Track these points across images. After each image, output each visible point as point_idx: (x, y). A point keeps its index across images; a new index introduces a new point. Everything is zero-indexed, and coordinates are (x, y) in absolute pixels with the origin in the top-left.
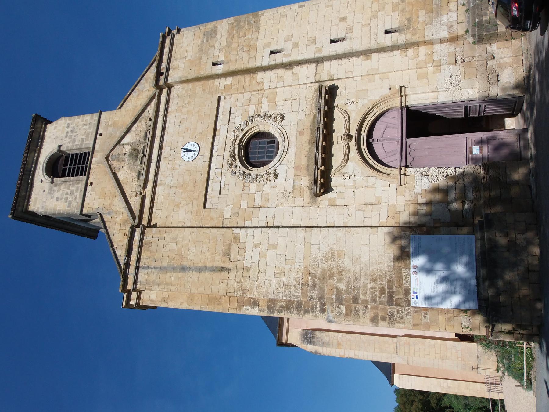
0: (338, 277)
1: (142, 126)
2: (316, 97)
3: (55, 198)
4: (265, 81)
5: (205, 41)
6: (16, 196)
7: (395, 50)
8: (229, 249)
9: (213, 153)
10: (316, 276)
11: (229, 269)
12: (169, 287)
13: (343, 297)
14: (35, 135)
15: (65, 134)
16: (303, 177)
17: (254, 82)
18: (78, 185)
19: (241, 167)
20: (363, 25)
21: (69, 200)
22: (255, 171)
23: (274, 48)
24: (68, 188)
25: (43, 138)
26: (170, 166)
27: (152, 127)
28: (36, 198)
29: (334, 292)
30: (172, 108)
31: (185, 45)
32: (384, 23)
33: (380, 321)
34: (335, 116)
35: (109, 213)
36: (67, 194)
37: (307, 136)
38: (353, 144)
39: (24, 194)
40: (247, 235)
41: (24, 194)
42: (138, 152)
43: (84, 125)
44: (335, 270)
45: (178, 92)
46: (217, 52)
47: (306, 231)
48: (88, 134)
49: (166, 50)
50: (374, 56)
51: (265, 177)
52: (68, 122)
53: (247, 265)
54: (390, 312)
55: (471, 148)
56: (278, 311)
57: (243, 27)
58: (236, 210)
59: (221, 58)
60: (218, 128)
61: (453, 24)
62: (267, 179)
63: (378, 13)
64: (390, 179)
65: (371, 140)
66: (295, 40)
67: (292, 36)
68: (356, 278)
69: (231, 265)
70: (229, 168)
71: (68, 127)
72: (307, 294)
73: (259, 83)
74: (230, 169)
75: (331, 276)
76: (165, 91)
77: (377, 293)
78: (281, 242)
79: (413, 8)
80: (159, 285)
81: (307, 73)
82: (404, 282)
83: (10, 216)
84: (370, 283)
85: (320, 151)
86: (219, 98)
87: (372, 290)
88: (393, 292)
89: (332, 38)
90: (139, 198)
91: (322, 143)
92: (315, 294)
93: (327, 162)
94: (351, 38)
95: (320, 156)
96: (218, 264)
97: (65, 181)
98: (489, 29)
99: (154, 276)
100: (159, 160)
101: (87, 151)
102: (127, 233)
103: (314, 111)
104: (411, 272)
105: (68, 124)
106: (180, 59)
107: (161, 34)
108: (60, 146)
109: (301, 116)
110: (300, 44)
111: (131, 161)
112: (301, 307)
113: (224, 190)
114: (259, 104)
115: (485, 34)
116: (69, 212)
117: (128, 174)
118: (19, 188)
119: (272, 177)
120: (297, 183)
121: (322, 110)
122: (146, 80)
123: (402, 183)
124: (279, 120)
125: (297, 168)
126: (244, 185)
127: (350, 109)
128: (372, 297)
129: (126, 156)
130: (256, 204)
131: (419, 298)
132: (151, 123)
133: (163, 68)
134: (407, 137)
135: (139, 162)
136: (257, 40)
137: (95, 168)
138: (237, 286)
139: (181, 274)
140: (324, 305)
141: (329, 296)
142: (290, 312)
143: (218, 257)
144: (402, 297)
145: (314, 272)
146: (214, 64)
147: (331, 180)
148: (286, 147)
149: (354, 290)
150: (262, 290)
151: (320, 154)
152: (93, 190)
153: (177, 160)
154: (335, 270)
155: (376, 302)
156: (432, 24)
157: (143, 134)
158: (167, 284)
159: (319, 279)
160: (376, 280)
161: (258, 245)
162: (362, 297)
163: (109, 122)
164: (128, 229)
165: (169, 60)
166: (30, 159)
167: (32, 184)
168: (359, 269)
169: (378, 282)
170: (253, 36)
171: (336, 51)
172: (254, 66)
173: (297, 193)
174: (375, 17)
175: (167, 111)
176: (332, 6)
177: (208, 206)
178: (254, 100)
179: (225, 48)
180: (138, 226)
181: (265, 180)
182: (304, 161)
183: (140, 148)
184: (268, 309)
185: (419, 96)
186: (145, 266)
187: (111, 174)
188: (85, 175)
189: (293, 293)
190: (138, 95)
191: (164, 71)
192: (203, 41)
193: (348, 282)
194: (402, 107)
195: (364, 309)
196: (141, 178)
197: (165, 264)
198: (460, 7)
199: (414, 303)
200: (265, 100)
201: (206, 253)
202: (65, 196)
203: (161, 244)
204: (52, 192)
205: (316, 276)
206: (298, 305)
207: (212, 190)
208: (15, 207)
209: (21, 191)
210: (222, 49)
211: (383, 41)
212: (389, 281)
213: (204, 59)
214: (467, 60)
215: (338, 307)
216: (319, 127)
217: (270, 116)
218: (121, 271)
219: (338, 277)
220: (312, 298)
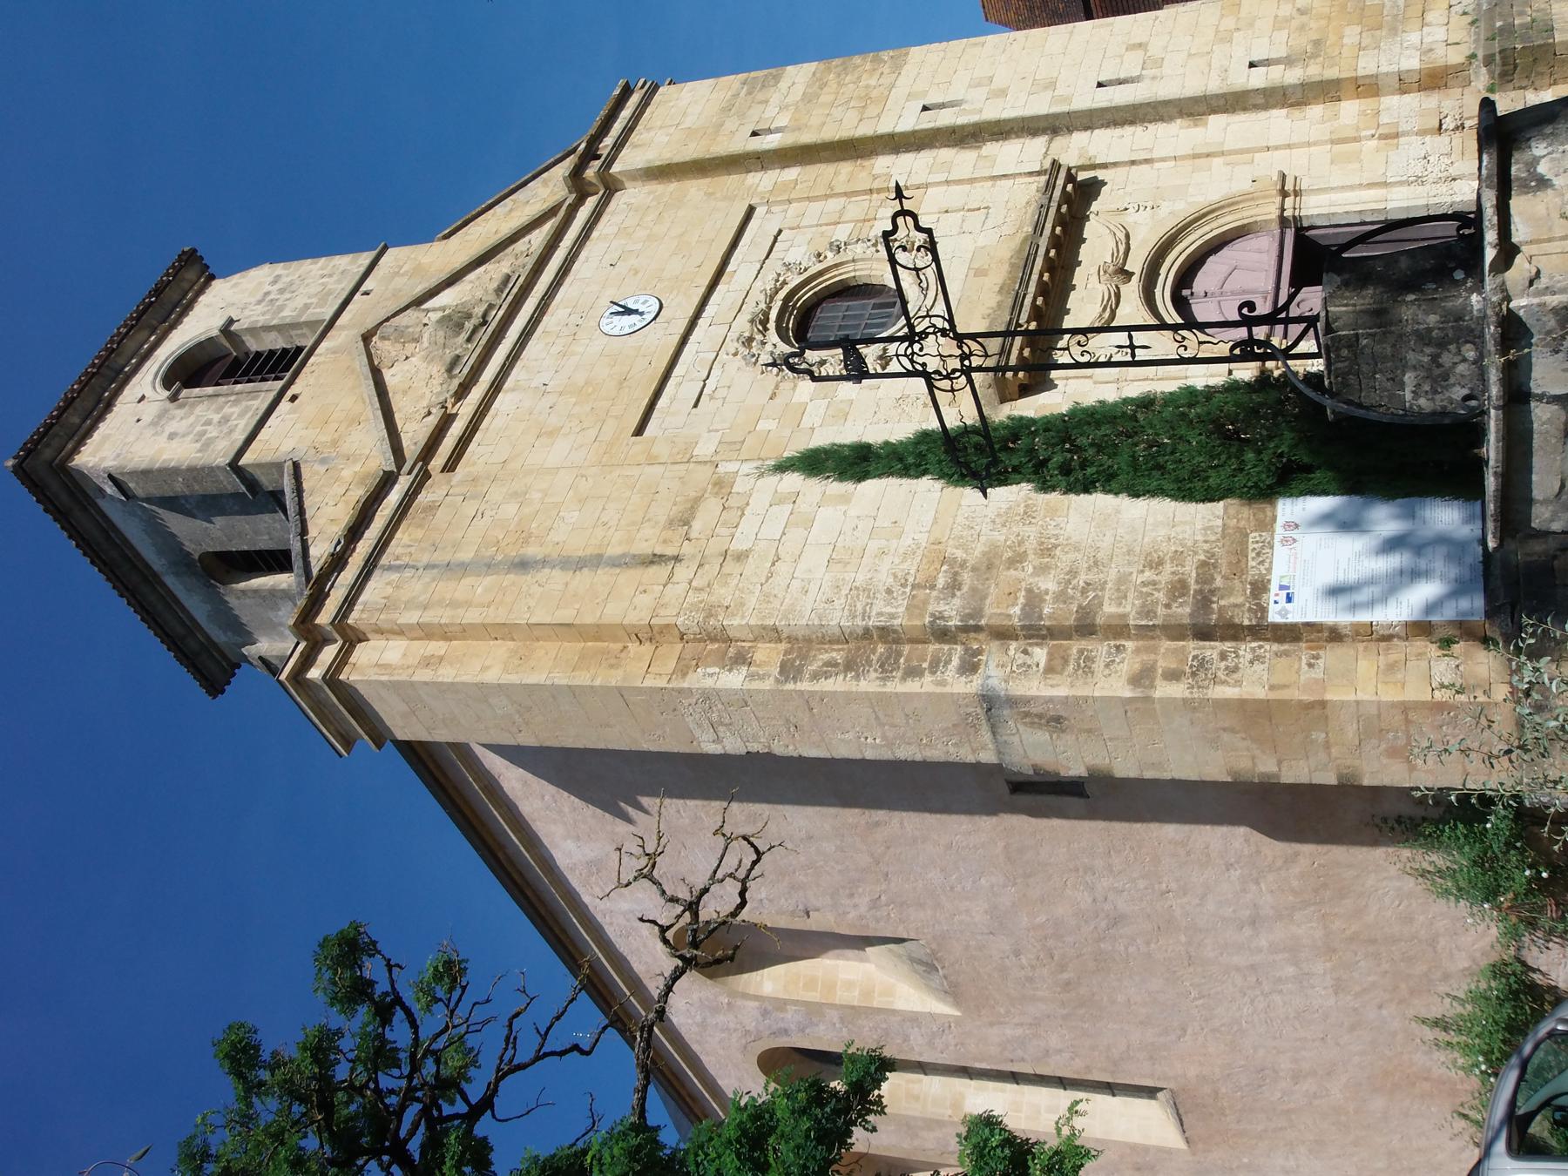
3: (166, 434)
6: (52, 417)
7: (1274, 107)
14: (171, 294)
15: (259, 296)
17: (864, 174)
20: (1190, 55)
39: (76, 420)
41: (76, 420)
44: (1031, 545)
49: (626, 113)
53: (738, 545)
56: (815, 676)
68: (1096, 563)
69: (687, 549)
75: (1017, 560)
76: (591, 202)
82: (1252, 563)
83: (10, 463)
85: (1032, 289)
86: (751, 210)
88: (1212, 592)
94: (1154, 78)
104: (1277, 538)
107: (622, 82)
108: (231, 321)
111: (441, 333)
112: (897, 661)
115: (1519, 46)
118: (70, 402)
127: (1127, 221)
128: (1144, 605)
131: (1295, 599)
138: (692, 598)
142: (857, 677)
144: (1240, 600)
145: (960, 554)
146: (754, 134)
149: (1084, 592)
150: (776, 603)
154: (1031, 545)
156: (1378, 47)
159: (974, 569)
160: (1160, 563)
166: (130, 345)
167: (109, 406)
168: (1108, 540)
169: (1168, 568)
177: (648, 432)
184: (781, 673)
185: (1334, 196)
187: (367, 370)
194: (1283, 222)
195: (1109, 653)
198: (1455, 19)
199: (1279, 613)
202: (199, 428)
203: (470, 509)
206: (888, 658)
209: (70, 410)
210: (787, 107)
215: (1025, 652)
218: (308, 581)
219: (1037, 562)
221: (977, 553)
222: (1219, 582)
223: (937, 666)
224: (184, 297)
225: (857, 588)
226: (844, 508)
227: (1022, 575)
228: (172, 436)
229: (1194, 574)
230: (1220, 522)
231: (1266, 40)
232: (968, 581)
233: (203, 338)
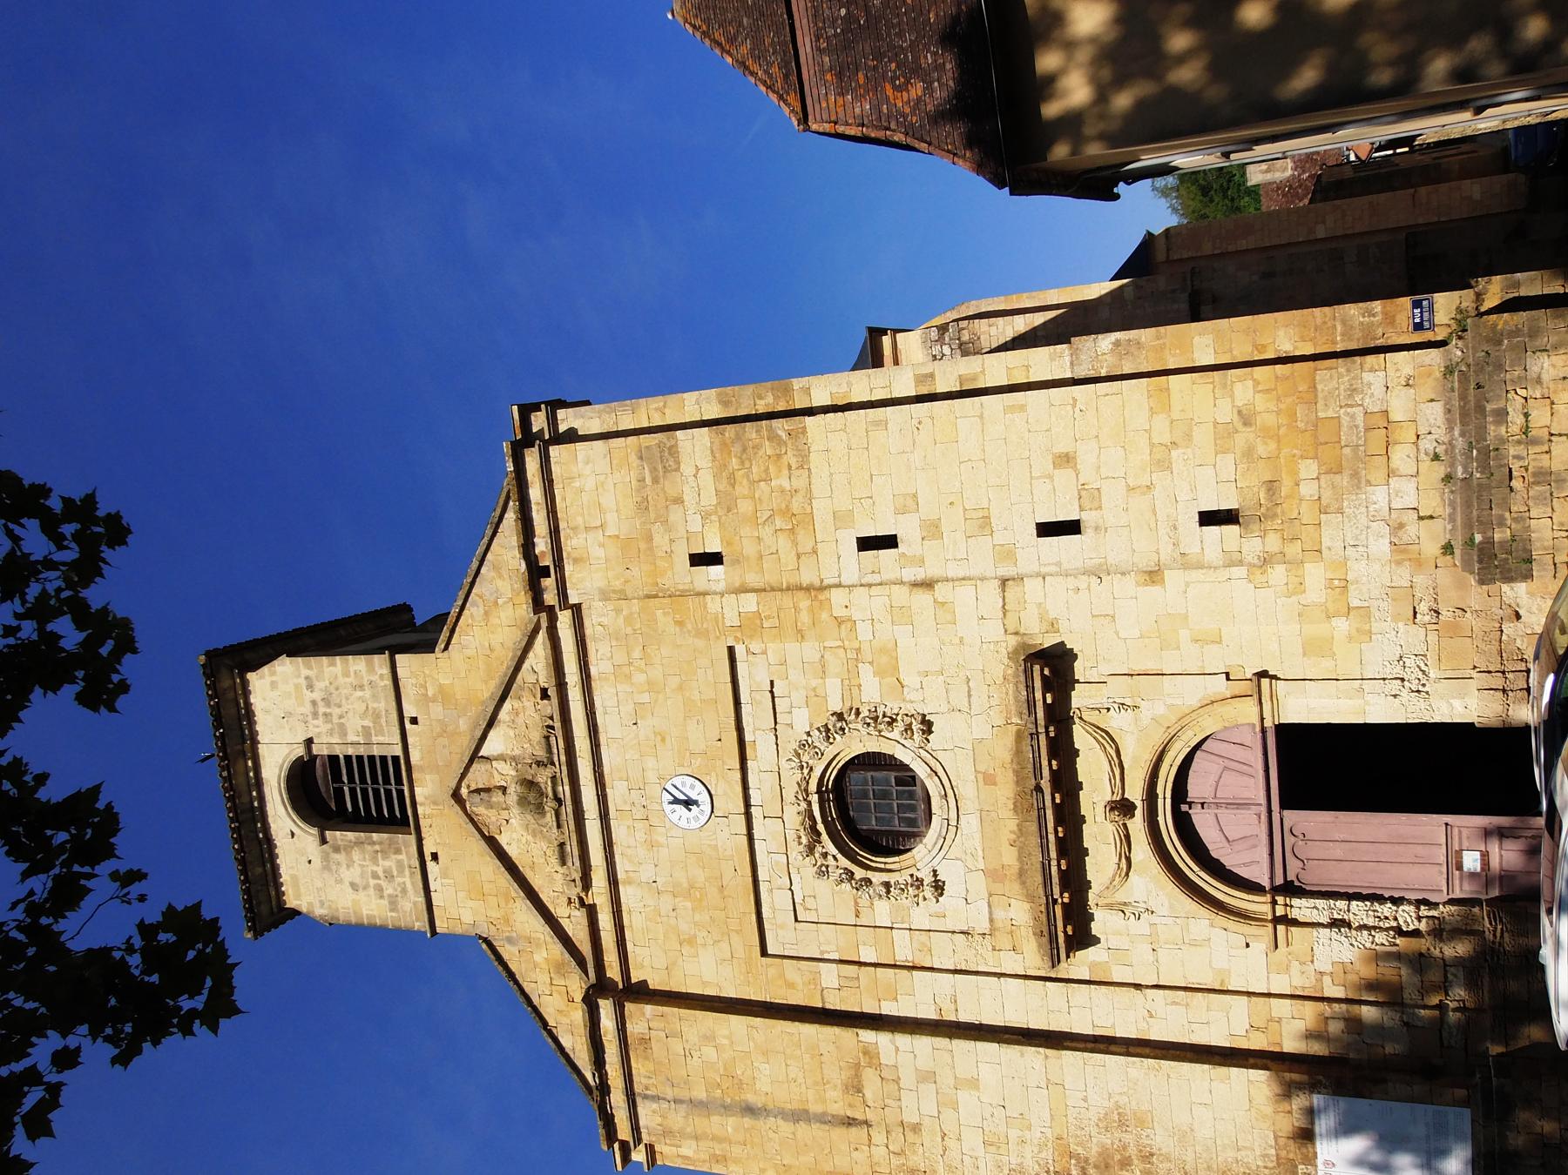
0: (1142, 1166)
2: (1016, 675)
5: (648, 481)
8: (858, 1075)
9: (753, 809)
11: (866, 1123)
16: (1013, 901)
17: (824, 616)
19: (839, 856)
20: (1130, 489)
24: (375, 861)
25: (250, 714)
27: (558, 725)
31: (590, 484)
32: (1194, 489)
34: (1087, 843)
35: (510, 940)
36: (375, 876)
37: (1005, 791)
38: (1137, 825)
39: (259, 870)
41: (259, 870)
42: (542, 794)
46: (695, 524)
49: (536, 493)
52: (305, 672)
53: (911, 1117)
55: (1459, 853)
60: (748, 737)
61: (1405, 519)
64: (1250, 929)
65: (1184, 808)
67: (915, 496)
69: (870, 1116)
71: (310, 687)
73: (840, 622)
76: (564, 619)
78: (987, 1074)
79: (1279, 449)
80: (697, 1138)
83: (249, 936)
85: (1053, 855)
91: (1056, 832)
93: (1075, 880)
95: (1054, 869)
96: (838, 1107)
98: (1510, 570)
103: (1015, 720)
108: (309, 742)
109: (981, 728)
116: (397, 924)
118: (242, 862)
119: (928, 892)
121: (1043, 738)
122: (496, 568)
126: (856, 903)
132: (552, 706)
134: (1286, 804)
135: (550, 818)
139: (747, 1121)
145: (1080, 1150)
147: (1091, 918)
151: (1054, 863)
153: (654, 821)
154: (1132, 1151)
156: (1340, 511)
159: (1096, 1167)
161: (929, 1077)
165: (555, 532)
166: (239, 781)
167: (269, 840)
170: (796, 483)
173: (1004, 941)
174: (1164, 465)
175: (588, 676)
179: (716, 513)
183: (543, 777)
190: (486, 613)
191: (547, 561)
197: (700, 1093)
198: (1426, 464)
200: (866, 672)
203: (677, 1046)
205: (1086, 1160)
208: (250, 910)
213: (660, 540)
214: (1446, 615)
216: (1038, 789)
221: (1094, 1152)
224: (238, 704)
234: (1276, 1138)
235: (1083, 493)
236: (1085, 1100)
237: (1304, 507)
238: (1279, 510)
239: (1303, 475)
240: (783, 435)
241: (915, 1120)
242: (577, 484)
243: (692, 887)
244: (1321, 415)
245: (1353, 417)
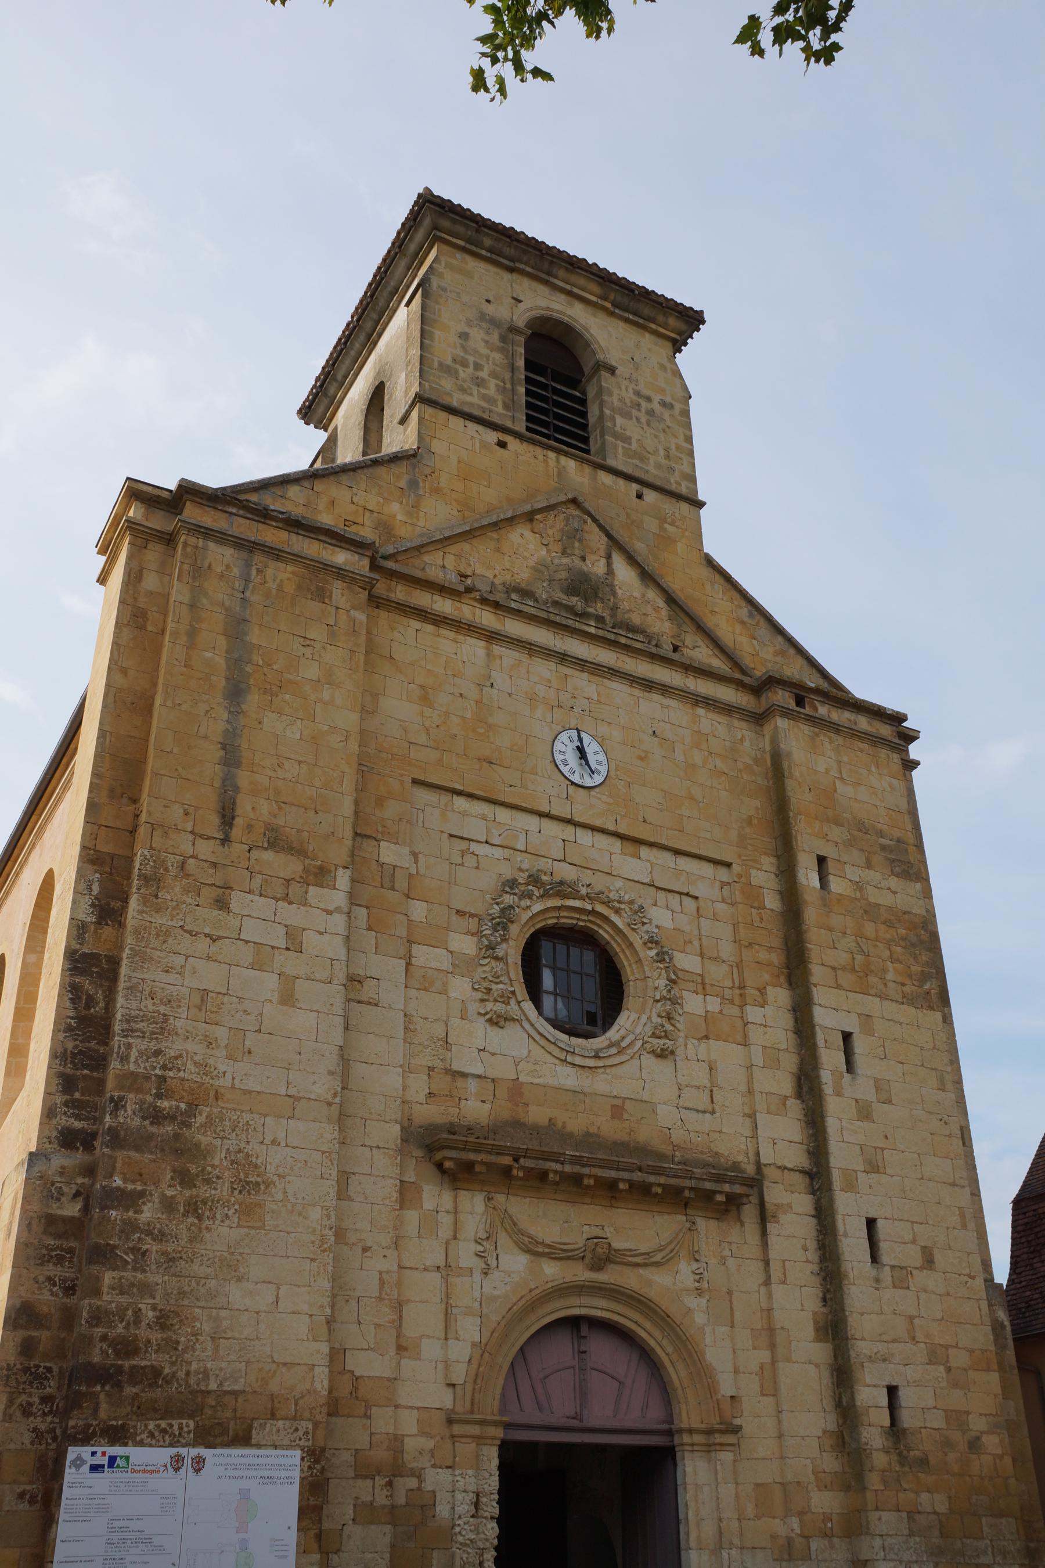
1: (660, 623)
3: (467, 330)
4: (769, 1010)
5: (882, 841)
10: (189, 1126)
11: (226, 841)
12: (183, 640)
13: (113, 1213)
15: (646, 392)
16: (487, 1107)
17: (767, 977)
18: (500, 404)
20: (911, 1318)
21: (460, 369)
22: (513, 951)
23: (860, 1045)
24: (493, 374)
26: (541, 690)
27: (654, 650)
28: (469, 275)
29: (133, 1182)
30: (703, 720)
33: (21, 1334)
35: (413, 484)
36: (478, 367)
38: (579, 1273)
40: (329, 912)
41: (488, 242)
43: (667, 450)
44: (204, 1191)
45: (747, 743)
46: (854, 873)
47: (329, 1104)
48: (642, 459)
50: (821, 1352)
51: (494, 987)
53: (237, 900)
54: (49, 1370)
57: (915, 958)
58: (401, 883)
59: (836, 885)
60: (644, 851)
62: (489, 990)
63: (941, 1368)
66: (879, 1109)
69: (238, 849)
70: (525, 875)
72: (130, 1090)
73: (762, 991)
74: (522, 877)
75: (184, 1178)
77: (120, 1329)
81: (781, 1140)
82: (151, 1425)
84: (154, 1308)
87: (130, 1312)
88: (119, 1385)
89: (880, 1224)
90: (451, 578)
91: (590, 1176)
92: (130, 1117)
94: (877, 1280)
96: (245, 807)
97: (513, 369)
99: (219, 593)
100: (563, 658)
101: (594, 446)
102: (353, 529)
104: (183, 1451)
105: (671, 407)
106: (839, 762)
108: (612, 370)
109: (667, 1115)
110: (866, 1124)
111: (563, 575)
112: (84, 1067)
113: (463, 853)
114: (703, 987)
117: (525, 558)
120: (472, 1085)
123: (457, 1429)
124: (658, 1043)
125: (516, 1089)
128: (107, 1313)
129: (578, 562)
130: (417, 950)
133: (816, 709)
135: (559, 596)
136: (883, 997)
137: (545, 461)
138: (172, 861)
140: (89, 1147)
141: (119, 1165)
143: (265, 808)
144: (102, 1414)
145: (201, 1119)
146: (821, 860)
148: (578, 1060)
149: (134, 1250)
150: (155, 943)
152: (484, 445)
154: (204, 1191)
155: (91, 1326)
157: (636, 619)
158: (192, 633)
159: (177, 1136)
160: (163, 1327)
161: (294, 942)
162: (108, 1278)
163: (672, 524)
164: (367, 533)
169: (156, 1336)
170: (891, 985)
171: (846, 1235)
172: (814, 979)
176: (964, 1226)
178: (718, 973)
180: (374, 566)
181: (485, 984)
182: (537, 1115)
186: (254, 572)
188: (528, 429)
189: (138, 1044)
190: (743, 623)
192: (881, 834)
193: (162, 1234)
195: (65, 1281)
196: (514, 596)
197: (255, 636)
199: (79, 1458)
200: (713, 1004)
201: (281, 773)
202: (471, 359)
203: (317, 633)
204: (484, 325)
205: (189, 1126)
207: (464, 814)
211: (868, 1381)
212: (157, 1372)
213: (837, 833)
215: (77, 1194)
217: (669, 1017)
220: (117, 1108)
221: (199, 1137)
222: (130, 1390)
223: (74, 1107)
225: (166, 1021)
226: (275, 1000)
227: (163, 1185)
228: (464, 336)
229: (143, 1363)
230: (213, 1386)
231: (931, 1403)
232: (162, 1130)
233: (595, 346)
234: (235, 1393)
235: (904, 1271)
236: (274, 1142)
237: (911, 1495)
238: (907, 1469)
239: (937, 1497)
240: (927, 987)
241: (234, 905)
242: (873, 769)
243: (490, 727)
244: (984, 1520)
245: (985, 1553)
